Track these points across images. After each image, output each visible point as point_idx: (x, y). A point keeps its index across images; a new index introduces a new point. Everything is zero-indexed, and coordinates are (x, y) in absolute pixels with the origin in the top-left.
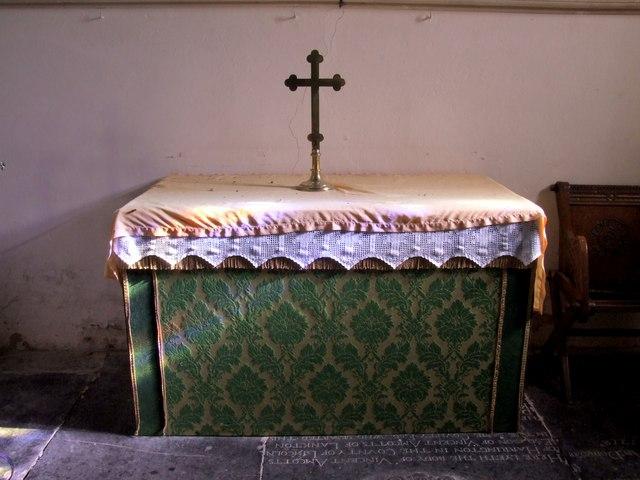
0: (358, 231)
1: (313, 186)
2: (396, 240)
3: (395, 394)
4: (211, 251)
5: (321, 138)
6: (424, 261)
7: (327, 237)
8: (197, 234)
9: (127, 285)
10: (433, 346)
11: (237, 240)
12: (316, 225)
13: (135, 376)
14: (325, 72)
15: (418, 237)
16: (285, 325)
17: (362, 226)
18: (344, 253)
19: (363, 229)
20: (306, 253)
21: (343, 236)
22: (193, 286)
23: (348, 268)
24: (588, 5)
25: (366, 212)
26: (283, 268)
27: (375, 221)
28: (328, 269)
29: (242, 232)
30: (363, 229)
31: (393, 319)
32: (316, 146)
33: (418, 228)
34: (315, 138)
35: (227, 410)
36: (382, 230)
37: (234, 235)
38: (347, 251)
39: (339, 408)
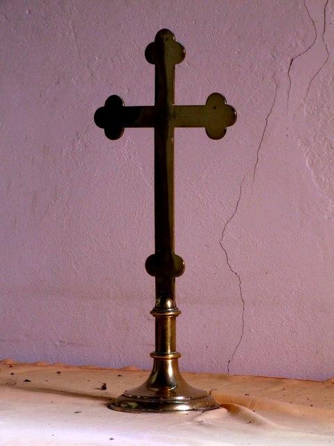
32: (165, 291)
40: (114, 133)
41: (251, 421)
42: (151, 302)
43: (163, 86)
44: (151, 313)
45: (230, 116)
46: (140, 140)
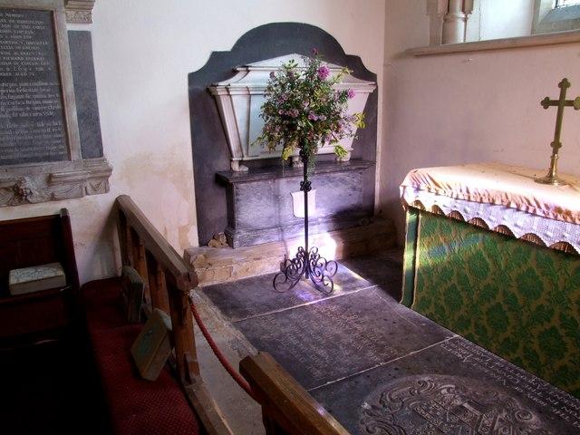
0: (527, 212)
1: (548, 180)
2: (552, 224)
3: (488, 321)
4: (446, 205)
5: (560, 145)
6: (571, 247)
7: (508, 211)
8: (440, 193)
9: (408, 214)
10: (513, 295)
11: (458, 201)
12: (502, 201)
13: (405, 268)
14: (555, 96)
15: (569, 226)
16: (478, 265)
17: (530, 209)
18: (516, 225)
19: (531, 211)
20: (493, 219)
21: (517, 213)
22: (435, 224)
23: (517, 237)
24: (472, 58)
25: (535, 199)
26: (479, 227)
27: (539, 207)
28: (505, 235)
29: (461, 197)
30: (531, 211)
31: (544, 286)
32: (555, 152)
33: (569, 219)
34: (556, 145)
35: (442, 307)
36: (543, 215)
37: (457, 199)
38: (520, 225)
39: (557, 364)
40: (546, 107)
41: (575, 190)
42: (551, 154)
43: (563, 94)
44: (91, 22)
45: (543, 103)
46: (554, 110)
